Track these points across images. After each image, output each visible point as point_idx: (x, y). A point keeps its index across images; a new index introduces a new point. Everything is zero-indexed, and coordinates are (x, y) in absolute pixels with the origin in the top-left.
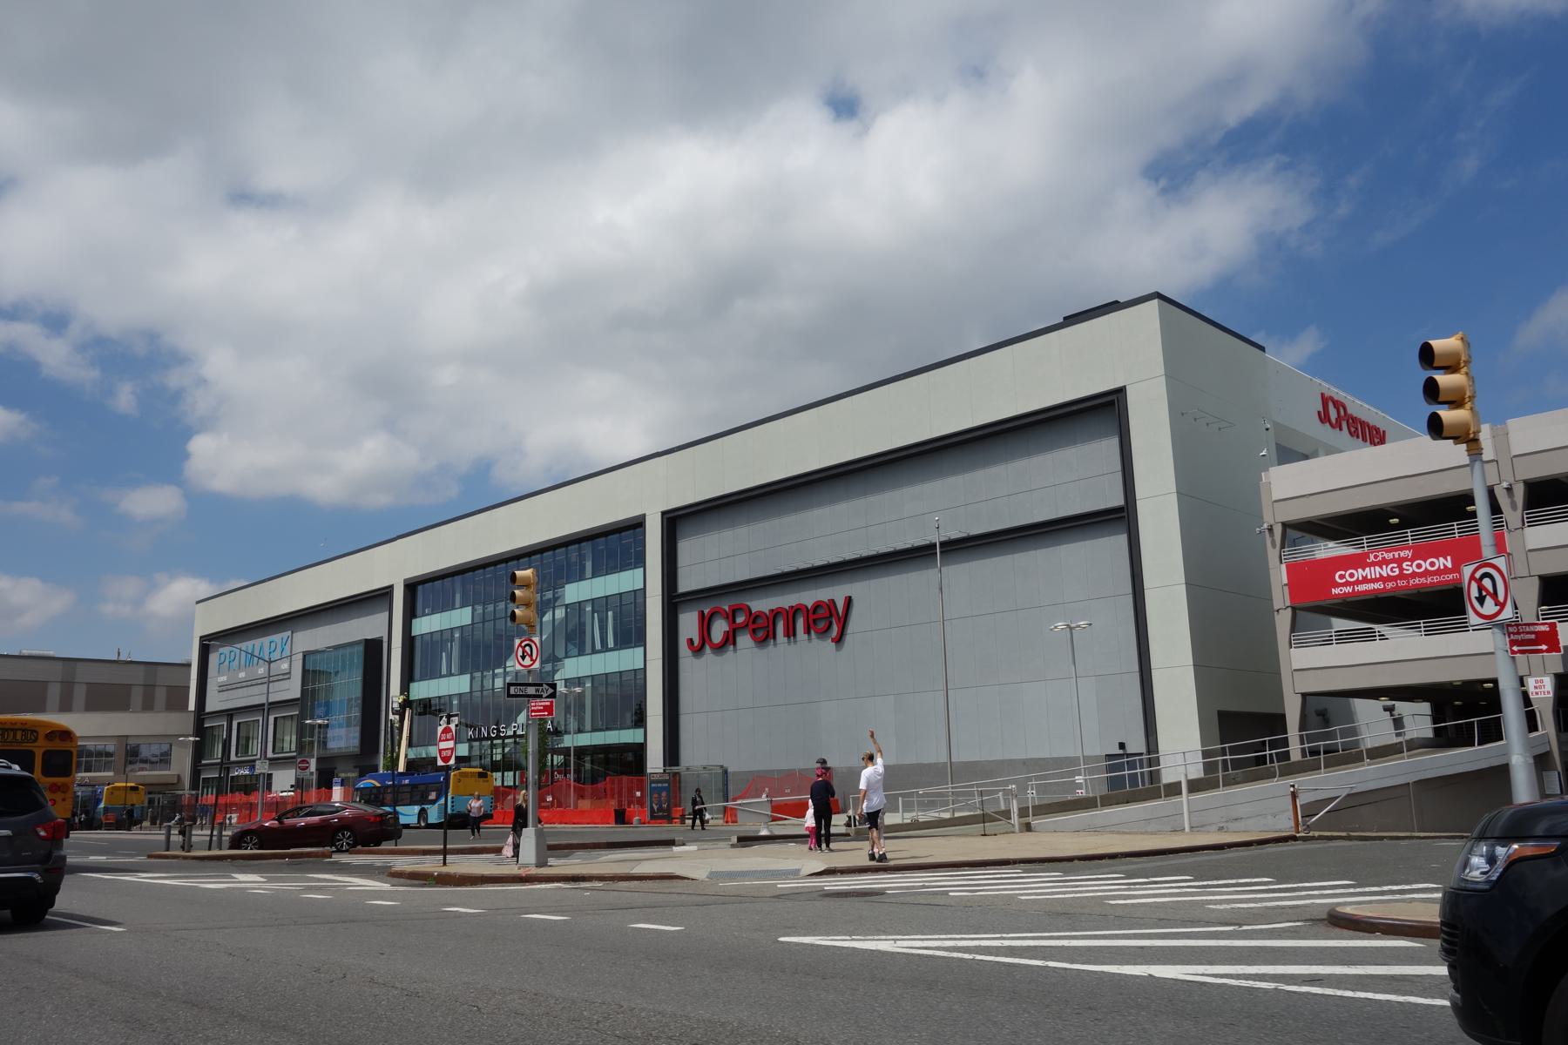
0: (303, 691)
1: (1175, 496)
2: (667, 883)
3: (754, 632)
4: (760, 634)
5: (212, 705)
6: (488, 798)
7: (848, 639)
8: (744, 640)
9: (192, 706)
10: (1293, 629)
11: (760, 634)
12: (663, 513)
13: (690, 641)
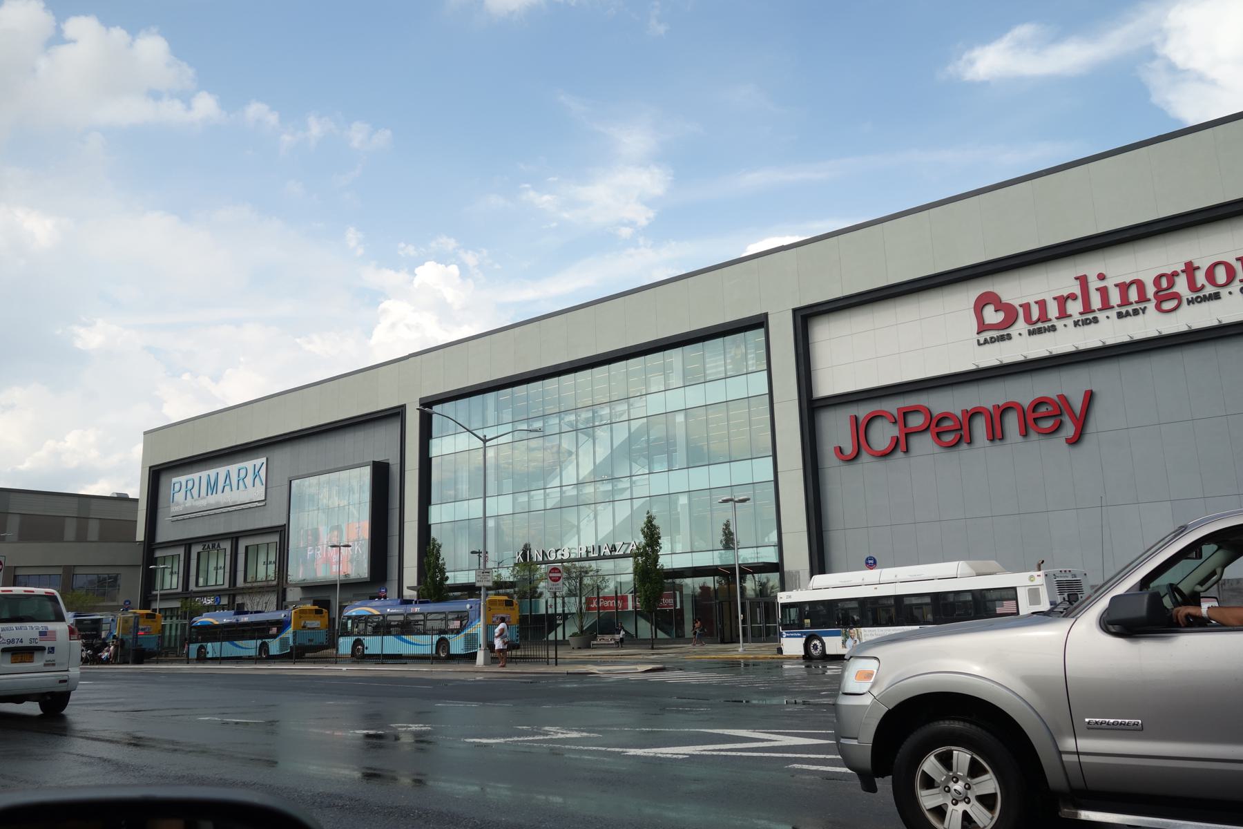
6: (515, 626)
8: (923, 445)
9: (140, 535)
12: (795, 311)
13: (840, 450)
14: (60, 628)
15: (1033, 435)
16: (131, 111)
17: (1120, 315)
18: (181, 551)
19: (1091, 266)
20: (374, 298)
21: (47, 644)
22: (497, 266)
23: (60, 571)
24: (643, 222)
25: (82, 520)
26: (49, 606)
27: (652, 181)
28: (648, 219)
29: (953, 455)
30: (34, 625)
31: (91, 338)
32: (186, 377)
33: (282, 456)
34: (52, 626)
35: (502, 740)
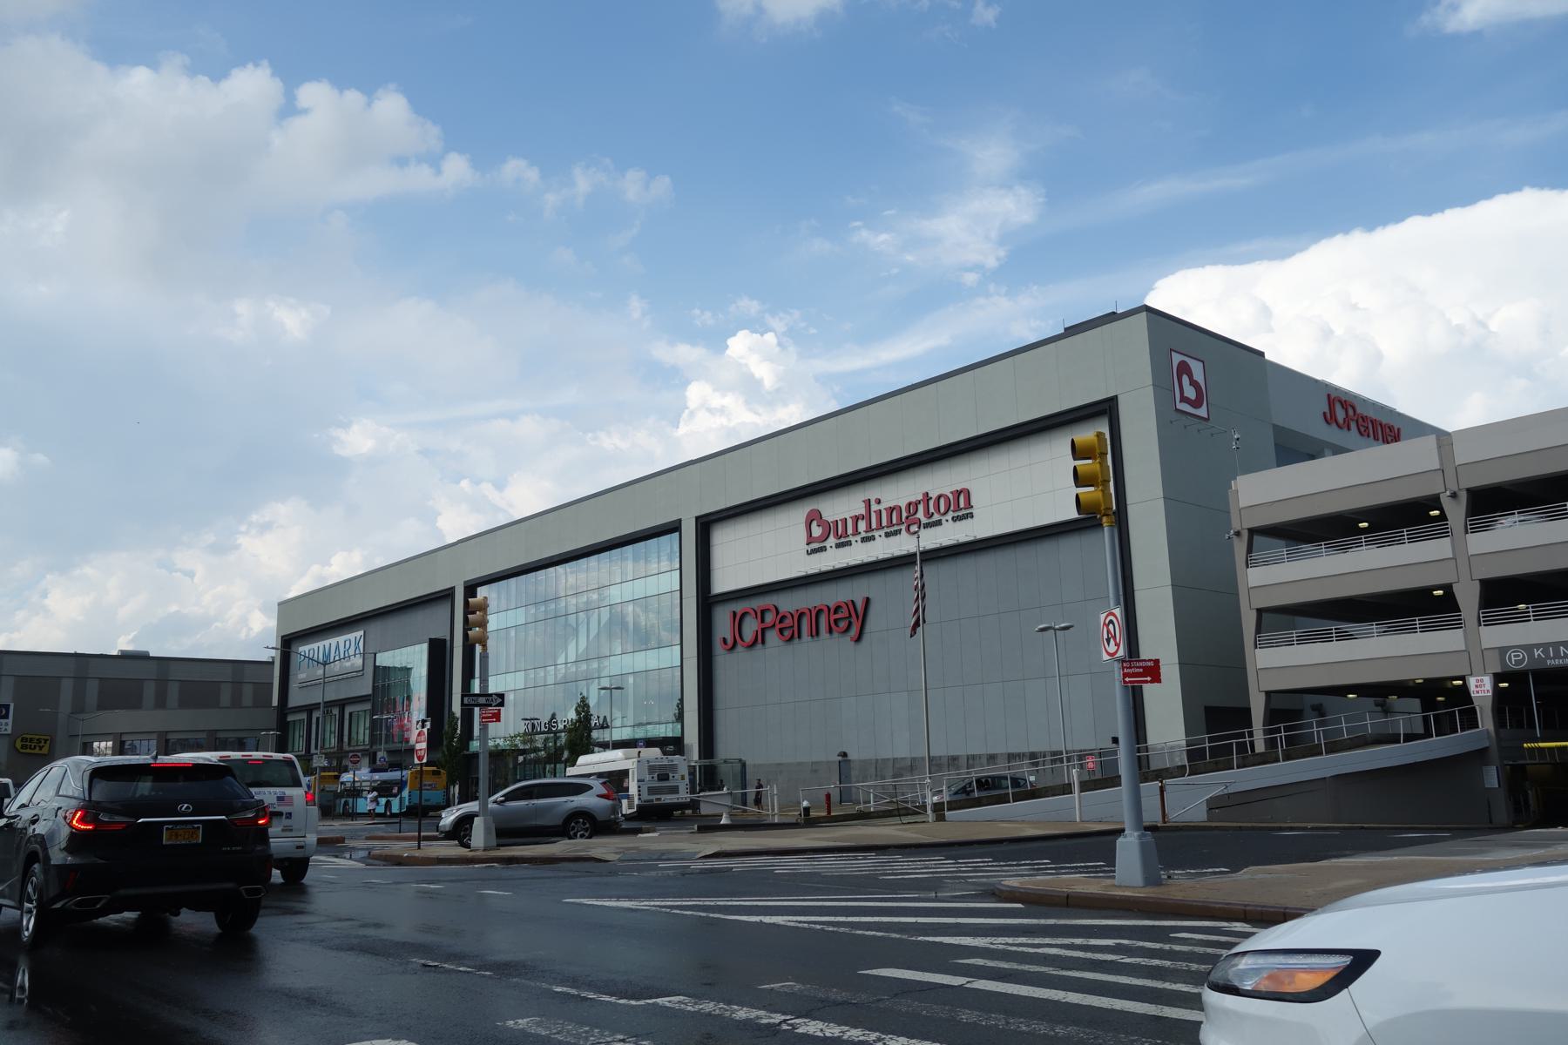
0: (374, 688)
1: (1162, 502)
2: (587, 865)
3: (781, 631)
4: (787, 633)
5: (295, 700)
7: (866, 637)
8: (772, 637)
9: (275, 702)
10: (1258, 630)
11: (787, 633)
12: (697, 518)
14: (297, 793)
15: (835, 635)
16: (378, 182)
17: (887, 535)
18: (304, 716)
19: (874, 491)
20: (675, 378)
21: (284, 809)
22: (813, 331)
23: (204, 735)
24: (991, 262)
25: (237, 684)
26: (287, 771)
27: (1016, 207)
28: (998, 259)
29: (790, 648)
30: (272, 790)
31: (359, 439)
32: (465, 483)
33: (376, 628)
34: (289, 791)
35: (585, 901)
